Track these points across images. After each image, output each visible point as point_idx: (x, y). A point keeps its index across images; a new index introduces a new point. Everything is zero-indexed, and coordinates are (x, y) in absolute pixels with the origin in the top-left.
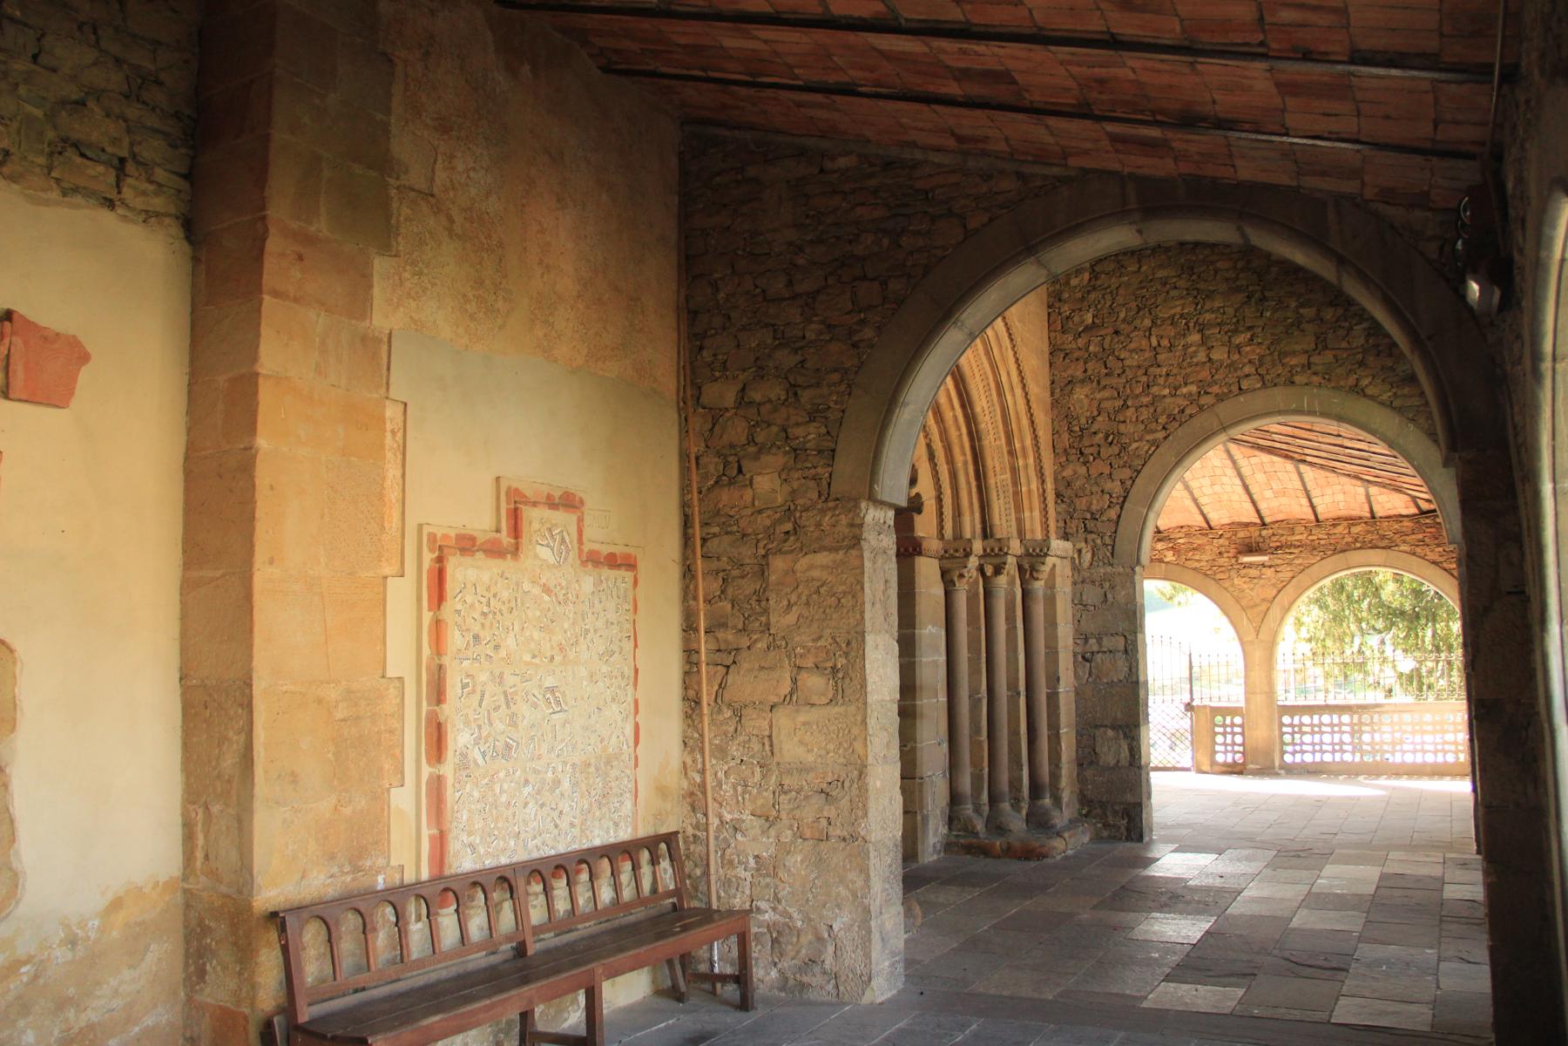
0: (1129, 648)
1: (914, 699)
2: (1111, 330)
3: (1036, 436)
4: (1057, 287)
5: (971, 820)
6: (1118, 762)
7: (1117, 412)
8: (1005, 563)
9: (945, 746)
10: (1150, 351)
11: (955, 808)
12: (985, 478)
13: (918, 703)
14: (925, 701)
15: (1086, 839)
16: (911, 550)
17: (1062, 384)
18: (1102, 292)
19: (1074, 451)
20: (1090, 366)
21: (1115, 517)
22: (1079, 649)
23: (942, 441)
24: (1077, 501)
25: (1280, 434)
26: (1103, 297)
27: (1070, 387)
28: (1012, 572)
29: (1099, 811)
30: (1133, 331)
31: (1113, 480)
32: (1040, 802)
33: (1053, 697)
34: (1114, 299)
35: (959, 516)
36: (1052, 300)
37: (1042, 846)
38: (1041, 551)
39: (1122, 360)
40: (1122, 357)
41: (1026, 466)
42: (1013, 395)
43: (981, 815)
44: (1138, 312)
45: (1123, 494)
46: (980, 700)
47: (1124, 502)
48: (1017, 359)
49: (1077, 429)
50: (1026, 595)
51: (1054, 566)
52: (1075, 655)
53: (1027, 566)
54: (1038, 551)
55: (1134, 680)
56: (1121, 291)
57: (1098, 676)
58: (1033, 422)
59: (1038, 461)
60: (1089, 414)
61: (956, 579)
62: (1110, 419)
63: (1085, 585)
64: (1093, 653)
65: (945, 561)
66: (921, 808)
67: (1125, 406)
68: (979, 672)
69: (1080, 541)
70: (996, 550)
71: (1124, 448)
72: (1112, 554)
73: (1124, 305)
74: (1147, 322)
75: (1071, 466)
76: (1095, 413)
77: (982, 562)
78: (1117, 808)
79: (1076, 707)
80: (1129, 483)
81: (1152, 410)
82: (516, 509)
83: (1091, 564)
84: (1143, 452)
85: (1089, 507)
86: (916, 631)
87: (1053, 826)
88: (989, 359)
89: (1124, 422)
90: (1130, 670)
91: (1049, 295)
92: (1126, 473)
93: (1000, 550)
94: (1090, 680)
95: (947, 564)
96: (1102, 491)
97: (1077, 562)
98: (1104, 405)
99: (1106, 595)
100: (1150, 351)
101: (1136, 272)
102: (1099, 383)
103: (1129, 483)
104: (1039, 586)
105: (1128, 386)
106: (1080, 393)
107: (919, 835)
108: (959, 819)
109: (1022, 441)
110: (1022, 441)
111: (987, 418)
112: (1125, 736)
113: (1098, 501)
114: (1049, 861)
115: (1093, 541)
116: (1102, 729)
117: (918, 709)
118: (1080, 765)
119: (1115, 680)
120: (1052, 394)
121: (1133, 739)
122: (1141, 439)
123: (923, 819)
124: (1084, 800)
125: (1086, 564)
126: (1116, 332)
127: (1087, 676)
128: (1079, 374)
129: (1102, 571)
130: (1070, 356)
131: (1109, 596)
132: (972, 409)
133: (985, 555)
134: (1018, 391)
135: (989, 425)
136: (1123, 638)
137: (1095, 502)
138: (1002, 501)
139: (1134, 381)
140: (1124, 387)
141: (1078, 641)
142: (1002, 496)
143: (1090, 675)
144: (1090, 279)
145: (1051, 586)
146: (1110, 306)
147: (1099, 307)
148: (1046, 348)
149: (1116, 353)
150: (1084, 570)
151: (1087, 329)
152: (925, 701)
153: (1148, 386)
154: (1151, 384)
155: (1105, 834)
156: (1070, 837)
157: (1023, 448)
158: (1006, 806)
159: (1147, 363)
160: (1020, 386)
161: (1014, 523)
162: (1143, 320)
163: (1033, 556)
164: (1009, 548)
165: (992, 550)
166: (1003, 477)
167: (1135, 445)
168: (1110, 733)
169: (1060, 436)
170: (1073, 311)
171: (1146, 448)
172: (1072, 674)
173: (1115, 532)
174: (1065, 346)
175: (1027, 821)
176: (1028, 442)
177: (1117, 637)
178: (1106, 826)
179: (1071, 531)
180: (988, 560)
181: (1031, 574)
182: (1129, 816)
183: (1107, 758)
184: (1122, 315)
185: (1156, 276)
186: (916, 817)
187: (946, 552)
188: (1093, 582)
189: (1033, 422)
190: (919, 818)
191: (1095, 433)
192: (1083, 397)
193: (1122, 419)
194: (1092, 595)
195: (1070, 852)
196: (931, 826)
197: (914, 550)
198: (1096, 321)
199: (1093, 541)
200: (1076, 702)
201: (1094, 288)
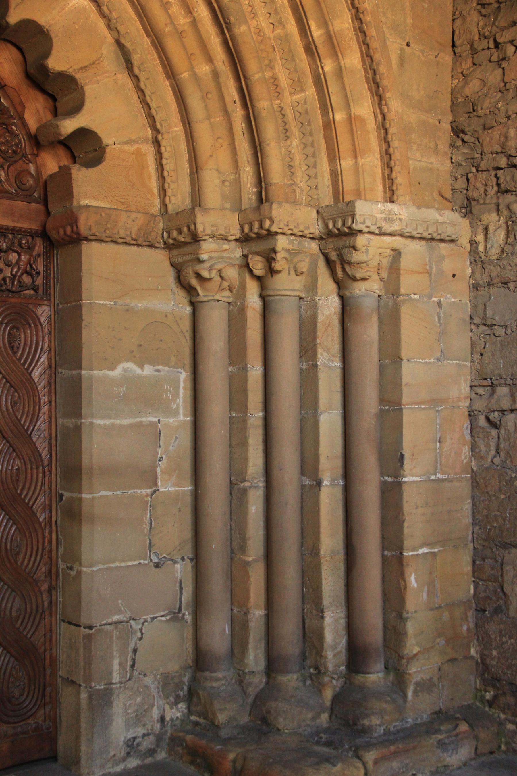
11: (199, 674)
12: (251, 101)
22: (479, 405)
23: (148, 35)
24: (486, 138)
32: (359, 678)
41: (339, 72)
51: (397, 253)
52: (472, 415)
53: (333, 256)
63: (492, 290)
64: (503, 411)
65: (175, 252)
66: (88, 679)
69: (489, 211)
82: (341, 254)
85: (503, 146)
94: (497, 460)
97: (481, 248)
117: (85, 508)
125: (494, 252)
127: (493, 452)
141: (481, 391)
142: (295, 131)
143: (498, 452)
150: (491, 262)
156: (376, 762)
169: (464, 19)
172: (466, 450)
186: (79, 693)
190: (84, 696)
200: (473, 498)
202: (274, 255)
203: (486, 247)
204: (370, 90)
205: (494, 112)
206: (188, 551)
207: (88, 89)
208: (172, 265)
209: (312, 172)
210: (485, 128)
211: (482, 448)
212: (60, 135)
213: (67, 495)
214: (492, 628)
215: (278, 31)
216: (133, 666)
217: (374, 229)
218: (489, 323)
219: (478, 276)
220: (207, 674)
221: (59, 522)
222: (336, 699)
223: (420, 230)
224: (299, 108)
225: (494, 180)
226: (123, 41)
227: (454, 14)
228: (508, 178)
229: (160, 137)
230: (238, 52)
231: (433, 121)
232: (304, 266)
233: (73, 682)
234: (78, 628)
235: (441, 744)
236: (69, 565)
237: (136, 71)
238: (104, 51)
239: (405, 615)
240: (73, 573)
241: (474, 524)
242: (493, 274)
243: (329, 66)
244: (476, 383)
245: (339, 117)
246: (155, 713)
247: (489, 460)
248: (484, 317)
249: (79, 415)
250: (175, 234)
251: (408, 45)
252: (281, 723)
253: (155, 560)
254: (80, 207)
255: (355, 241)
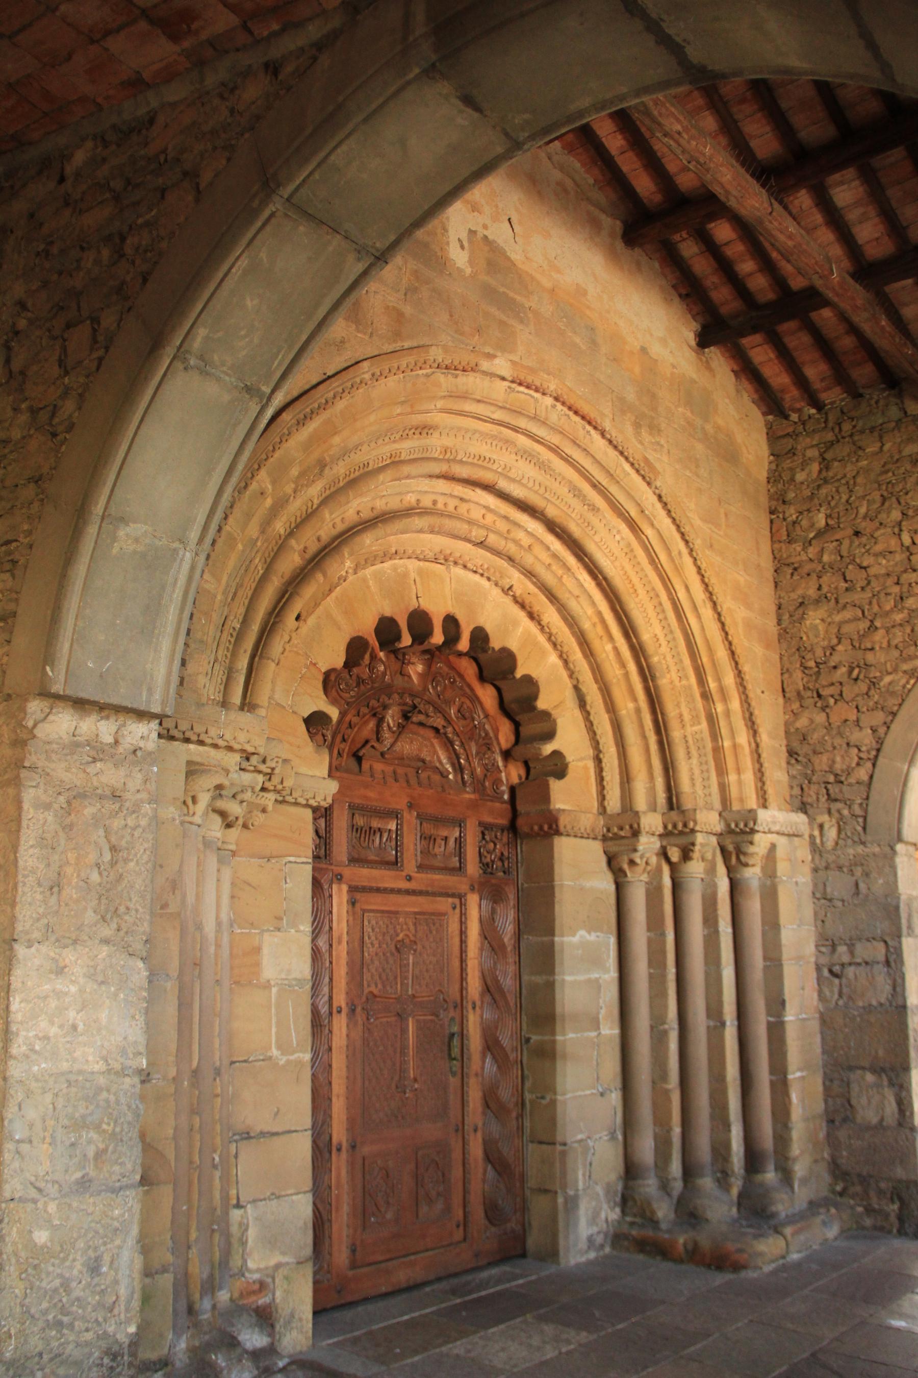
0: (891, 960)
1: (553, 1033)
2: (849, 532)
3: (740, 672)
4: (780, 486)
5: (649, 1204)
6: (882, 1119)
7: (862, 637)
8: (693, 844)
9: (615, 1097)
10: (902, 552)
11: (631, 1183)
12: (666, 730)
13: (559, 1038)
14: (571, 1035)
15: (832, 1232)
16: (546, 827)
17: (791, 608)
18: (836, 484)
19: (809, 693)
20: (825, 579)
21: (865, 778)
22: (824, 960)
23: (596, 682)
24: (816, 760)
25: (226, 275)
26: (837, 491)
27: (800, 611)
28: (709, 856)
29: (858, 1189)
30: (878, 529)
31: (861, 728)
32: (759, 1178)
33: (776, 1030)
34: (851, 491)
35: (628, 782)
36: (774, 503)
37: (740, 1251)
38: (746, 825)
39: (865, 568)
40: (865, 564)
41: (728, 713)
42: (699, 617)
43: (669, 1195)
44: (883, 504)
45: (875, 745)
46: (665, 1033)
47: (876, 757)
48: (699, 568)
49: (812, 664)
50: (735, 887)
51: (773, 847)
52: (818, 968)
53: (731, 848)
54: (742, 825)
55: (900, 1003)
56: (859, 480)
57: (850, 998)
58: (733, 653)
59: (746, 705)
60: (826, 643)
61: (625, 866)
62: (854, 647)
63: (830, 873)
64: (843, 965)
65: (610, 843)
66: (564, 1186)
67: (872, 628)
68: (664, 994)
69: (822, 813)
70: (680, 826)
71: (873, 684)
72: (864, 828)
73: (864, 497)
74: (896, 515)
75: (806, 714)
76: (835, 641)
77: (664, 843)
78: (883, 1185)
79: (823, 1039)
80: (882, 730)
81: (908, 630)
83: (837, 844)
84: (898, 688)
85: (831, 767)
86: (556, 939)
87: (773, 1215)
88: (656, 569)
89: (872, 649)
90: (894, 988)
91: (771, 498)
92: (879, 717)
93: (685, 825)
94: (841, 1003)
95: (613, 848)
96: (848, 744)
97: (818, 841)
98: (847, 629)
99: (857, 885)
100: (902, 552)
101: (877, 454)
102: (837, 602)
103: (882, 730)
104: (752, 874)
105: (874, 601)
106: (815, 618)
107: (561, 1224)
108: (635, 1201)
109: (719, 680)
110: (719, 680)
111: (664, 649)
112: (891, 1084)
113: (842, 757)
114: (751, 1274)
115: (839, 811)
116: (859, 1072)
117: (559, 1047)
118: (831, 1121)
119: (874, 1003)
120: (779, 624)
121: (901, 1087)
122: (895, 670)
123: (566, 1202)
124: (837, 1171)
125: (830, 844)
126: (857, 534)
127: (836, 996)
128: (812, 592)
129: (851, 851)
130: (799, 570)
131: (862, 886)
132: (637, 636)
133: (666, 835)
134: (707, 612)
135: (669, 658)
136: (882, 944)
137: (838, 759)
138: (695, 761)
139: (882, 595)
140: (870, 603)
141: (823, 949)
142: (694, 753)
143: (840, 995)
144: (820, 471)
145: (770, 871)
146: (847, 501)
147: (833, 504)
148: (767, 564)
149: (858, 560)
150: (828, 852)
151: (820, 534)
152: (571, 1035)
153: (902, 598)
154: (905, 595)
155: (868, 1222)
156: (793, 1235)
157: (722, 690)
158: (707, 1183)
159: (899, 569)
160: (709, 605)
161: (715, 789)
162: (889, 513)
163: (737, 833)
164: (695, 822)
165: (675, 826)
166: (695, 728)
167: (887, 679)
168: (870, 1077)
169: (791, 676)
170: (801, 513)
171: (903, 681)
172: (815, 995)
173: (867, 798)
174: (792, 560)
175: (739, 1205)
176: (729, 680)
177: (875, 943)
178: (869, 1210)
179: (810, 800)
180: (673, 840)
181: (738, 858)
182: (900, 1199)
183: (868, 1114)
184: (863, 510)
185: (904, 454)
187: (608, 830)
188: (840, 868)
189: (733, 653)
190: (560, 1200)
191: (835, 667)
192: (818, 621)
193: (869, 646)
194: (839, 885)
195: (795, 1256)
196: (584, 1210)
197: (550, 827)
198: (831, 522)
199: (839, 811)
200: (822, 1033)
201: (826, 481)
202: (692, 848)
203: (822, 840)
204: (746, 725)
205: (822, 742)
206: (618, 1083)
207: (560, 722)
208: (605, 852)
209: (706, 783)
210: (815, 752)
211: (828, 993)
212: (541, 755)
213: (535, 1038)
214: (842, 1134)
215: (684, 682)
216: (590, 1176)
217: (766, 830)
218: (829, 897)
219: (817, 861)
220: (640, 1182)
221: (525, 1061)
222: (740, 1195)
223: (789, 829)
224: (697, 736)
225: (825, 791)
226: (580, 686)
227: (782, 670)
228: (837, 790)
229: (601, 756)
230: (658, 696)
231: (777, 745)
232: (709, 856)
233: (546, 1191)
234: (550, 1147)
235: (824, 1223)
236: (539, 1095)
237: (588, 708)
238: (567, 694)
239: (790, 1125)
240: (544, 1102)
241: (824, 1052)
242: (830, 861)
243: (720, 708)
244: (820, 943)
245: (727, 744)
246: (603, 1215)
247: (834, 1002)
248: (825, 892)
249: (552, 972)
250: (616, 830)
251: (763, 692)
252: (709, 1215)
253: (601, 1090)
254: (559, 810)
255: (753, 838)
